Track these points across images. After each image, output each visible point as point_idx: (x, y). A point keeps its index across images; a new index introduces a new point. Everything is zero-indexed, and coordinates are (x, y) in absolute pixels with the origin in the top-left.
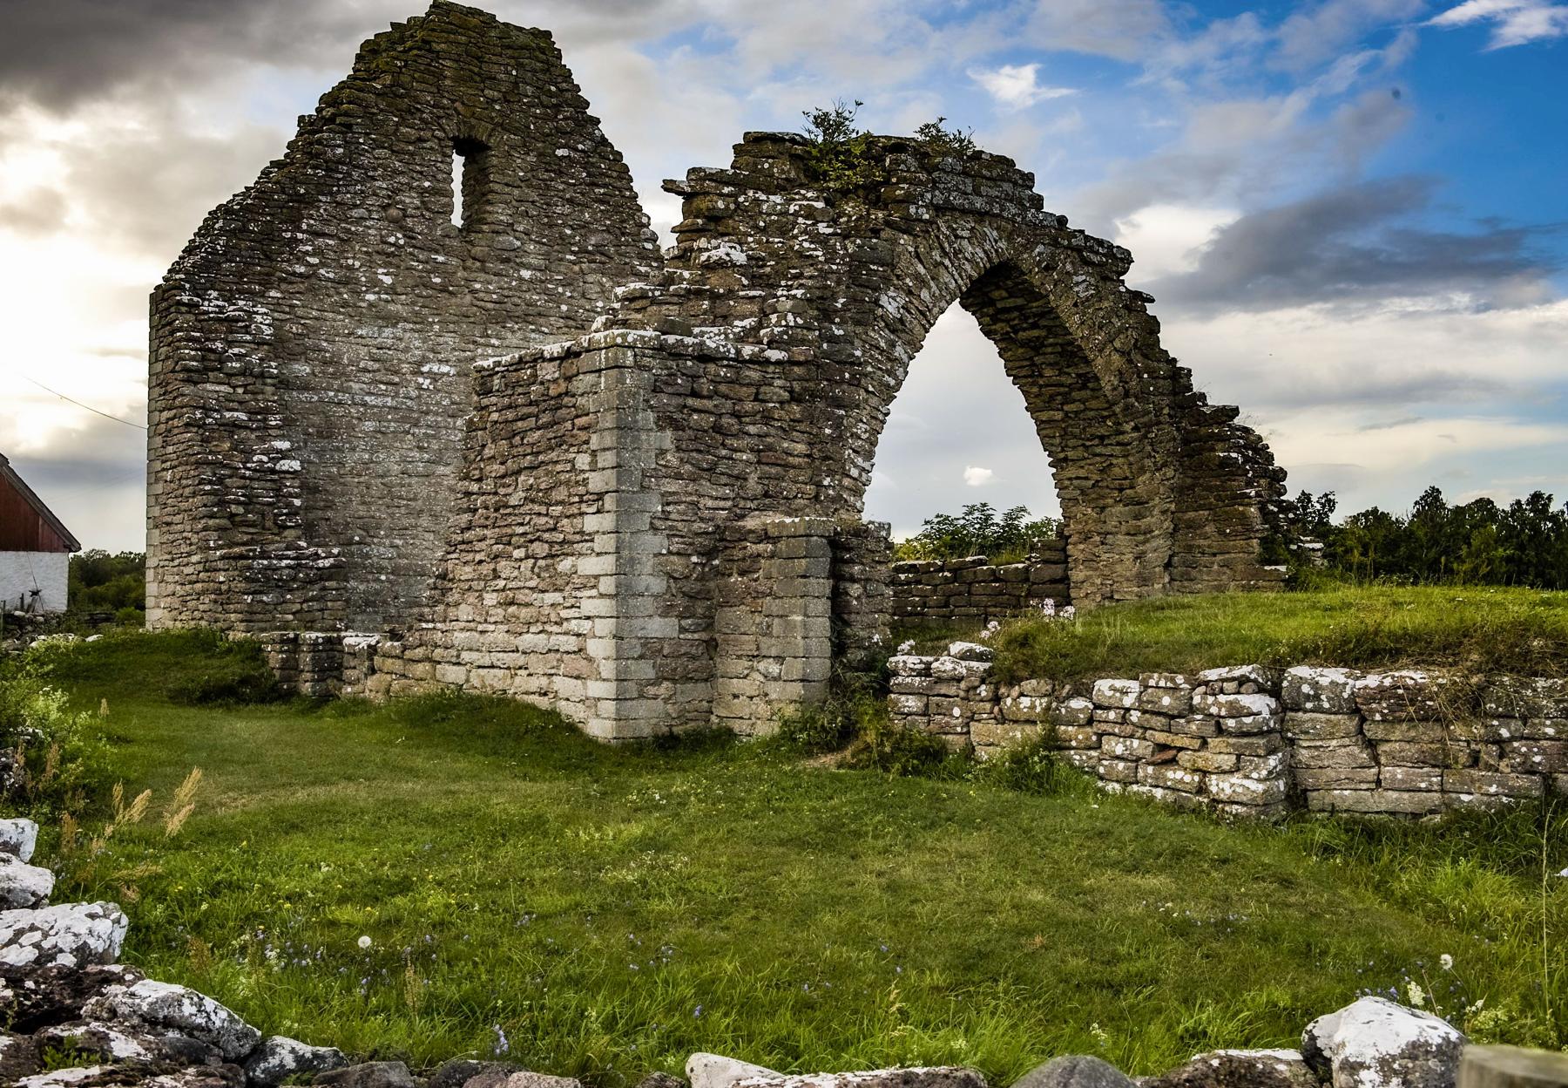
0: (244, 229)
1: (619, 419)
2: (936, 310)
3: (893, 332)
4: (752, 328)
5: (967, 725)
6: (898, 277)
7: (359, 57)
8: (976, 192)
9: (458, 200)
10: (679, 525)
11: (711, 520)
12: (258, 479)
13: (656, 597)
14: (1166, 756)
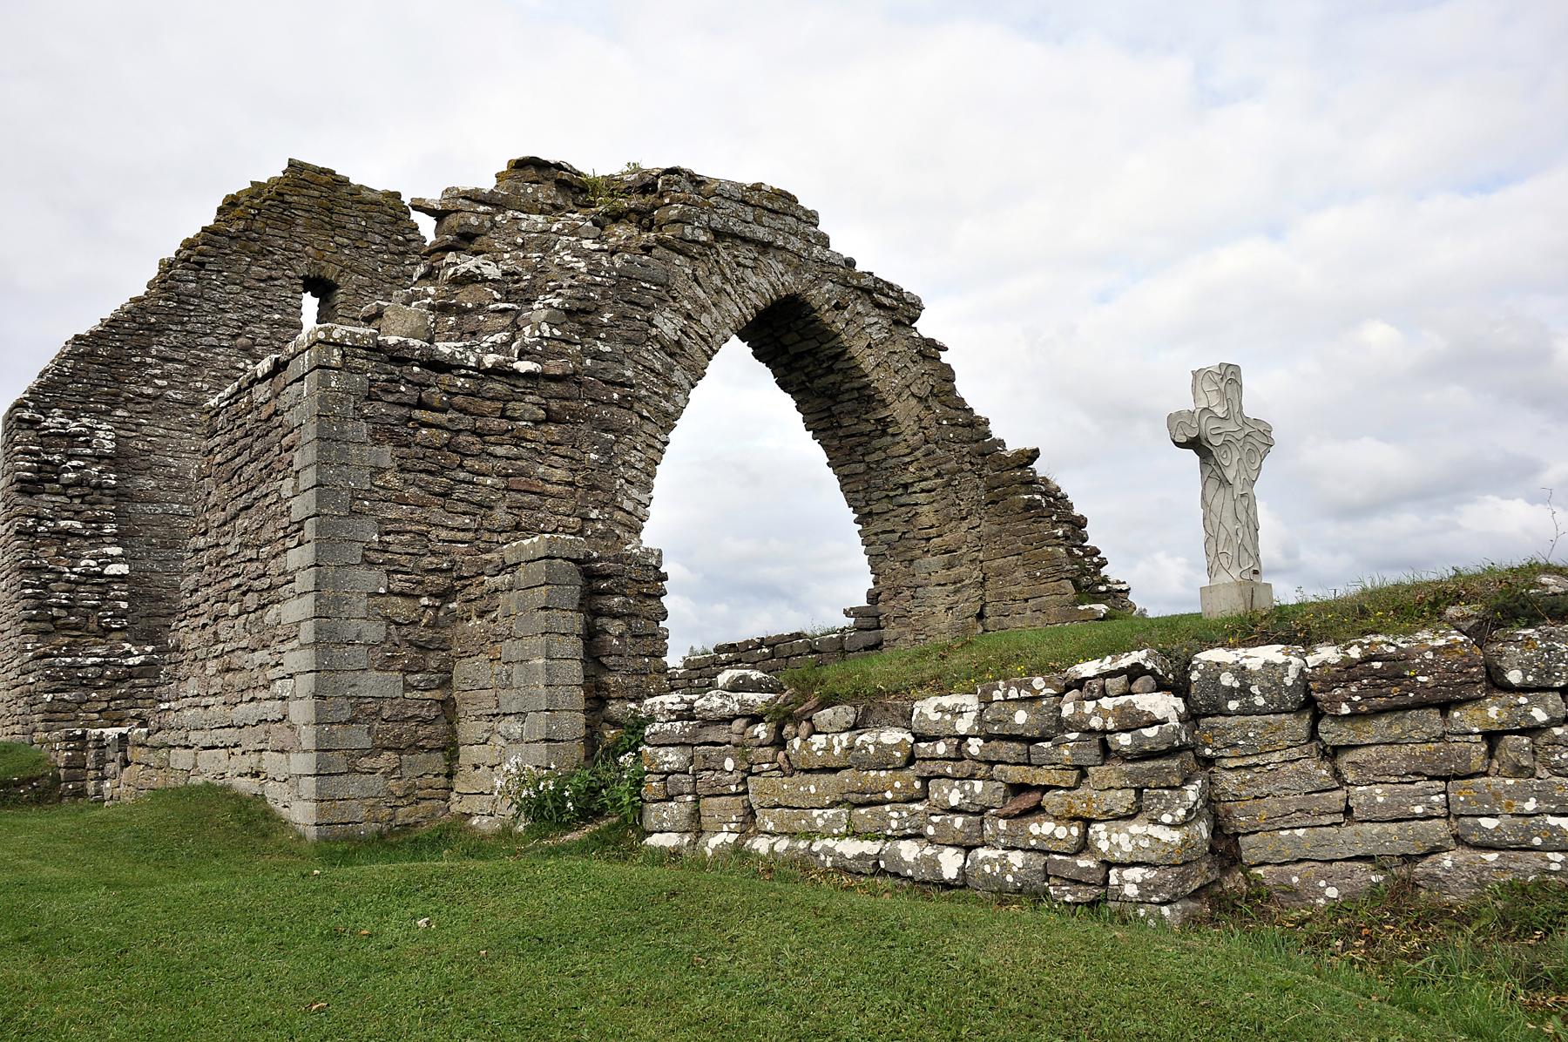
0: (91, 354)
1: (320, 428)
2: (719, 337)
3: (671, 355)
4: (504, 344)
5: (744, 780)
6: (674, 299)
7: (220, 210)
12: (84, 583)
13: (371, 646)
14: (1026, 800)
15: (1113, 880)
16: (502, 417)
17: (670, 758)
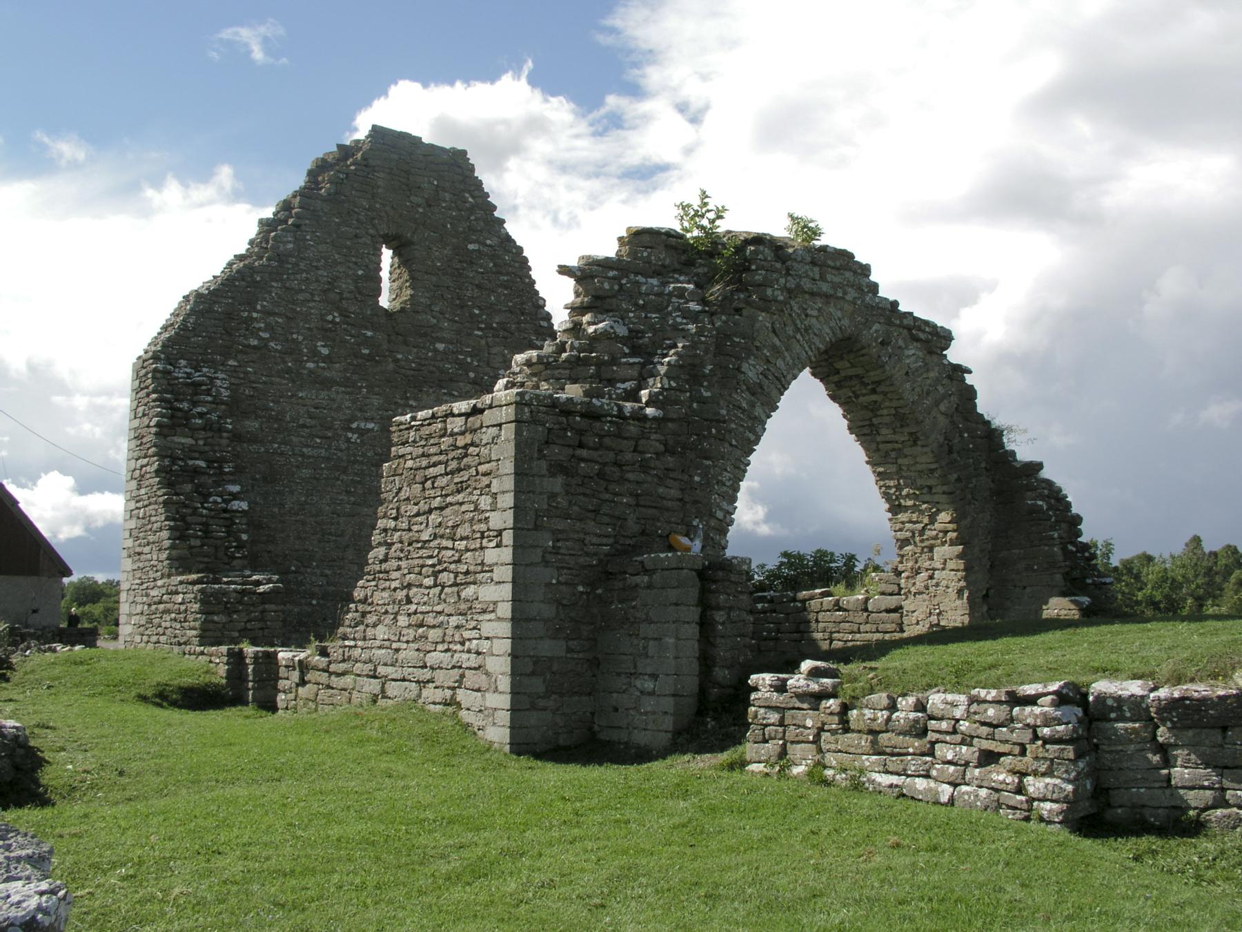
2: (789, 377)
3: (753, 394)
11: (595, 554)
13: (546, 621)
16: (634, 451)
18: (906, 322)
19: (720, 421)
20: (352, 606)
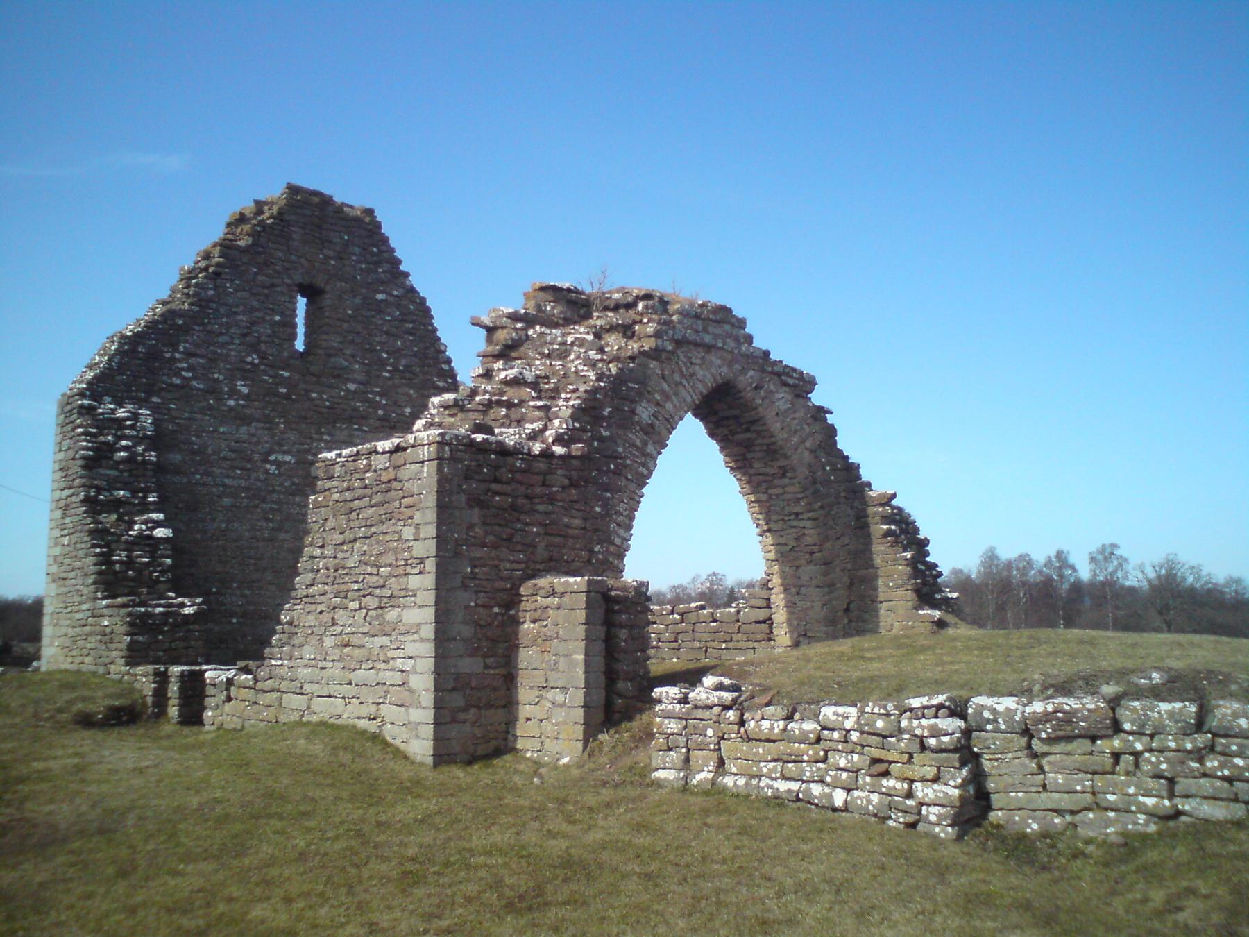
3: (646, 433)
5: (719, 743)
8: (705, 330)
9: (301, 330)
10: (485, 583)
11: (510, 578)
13: (465, 640)
15: (924, 812)
17: (672, 725)
18: (776, 369)
19: (616, 457)
20: (279, 627)
